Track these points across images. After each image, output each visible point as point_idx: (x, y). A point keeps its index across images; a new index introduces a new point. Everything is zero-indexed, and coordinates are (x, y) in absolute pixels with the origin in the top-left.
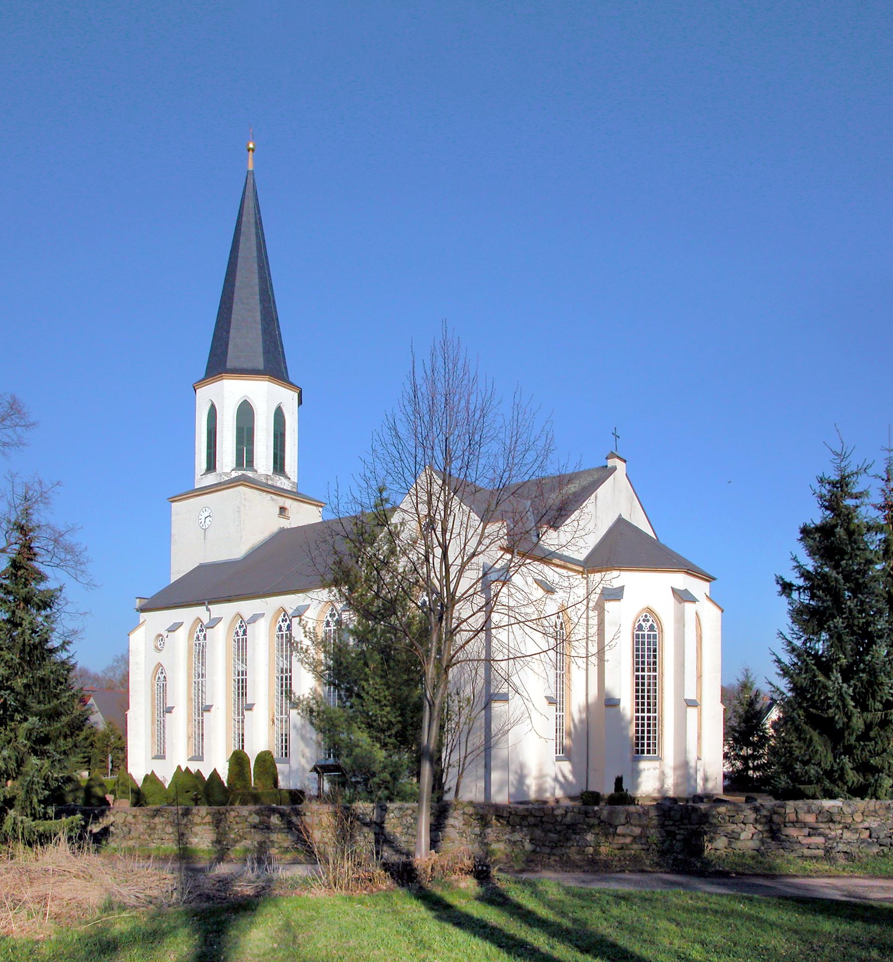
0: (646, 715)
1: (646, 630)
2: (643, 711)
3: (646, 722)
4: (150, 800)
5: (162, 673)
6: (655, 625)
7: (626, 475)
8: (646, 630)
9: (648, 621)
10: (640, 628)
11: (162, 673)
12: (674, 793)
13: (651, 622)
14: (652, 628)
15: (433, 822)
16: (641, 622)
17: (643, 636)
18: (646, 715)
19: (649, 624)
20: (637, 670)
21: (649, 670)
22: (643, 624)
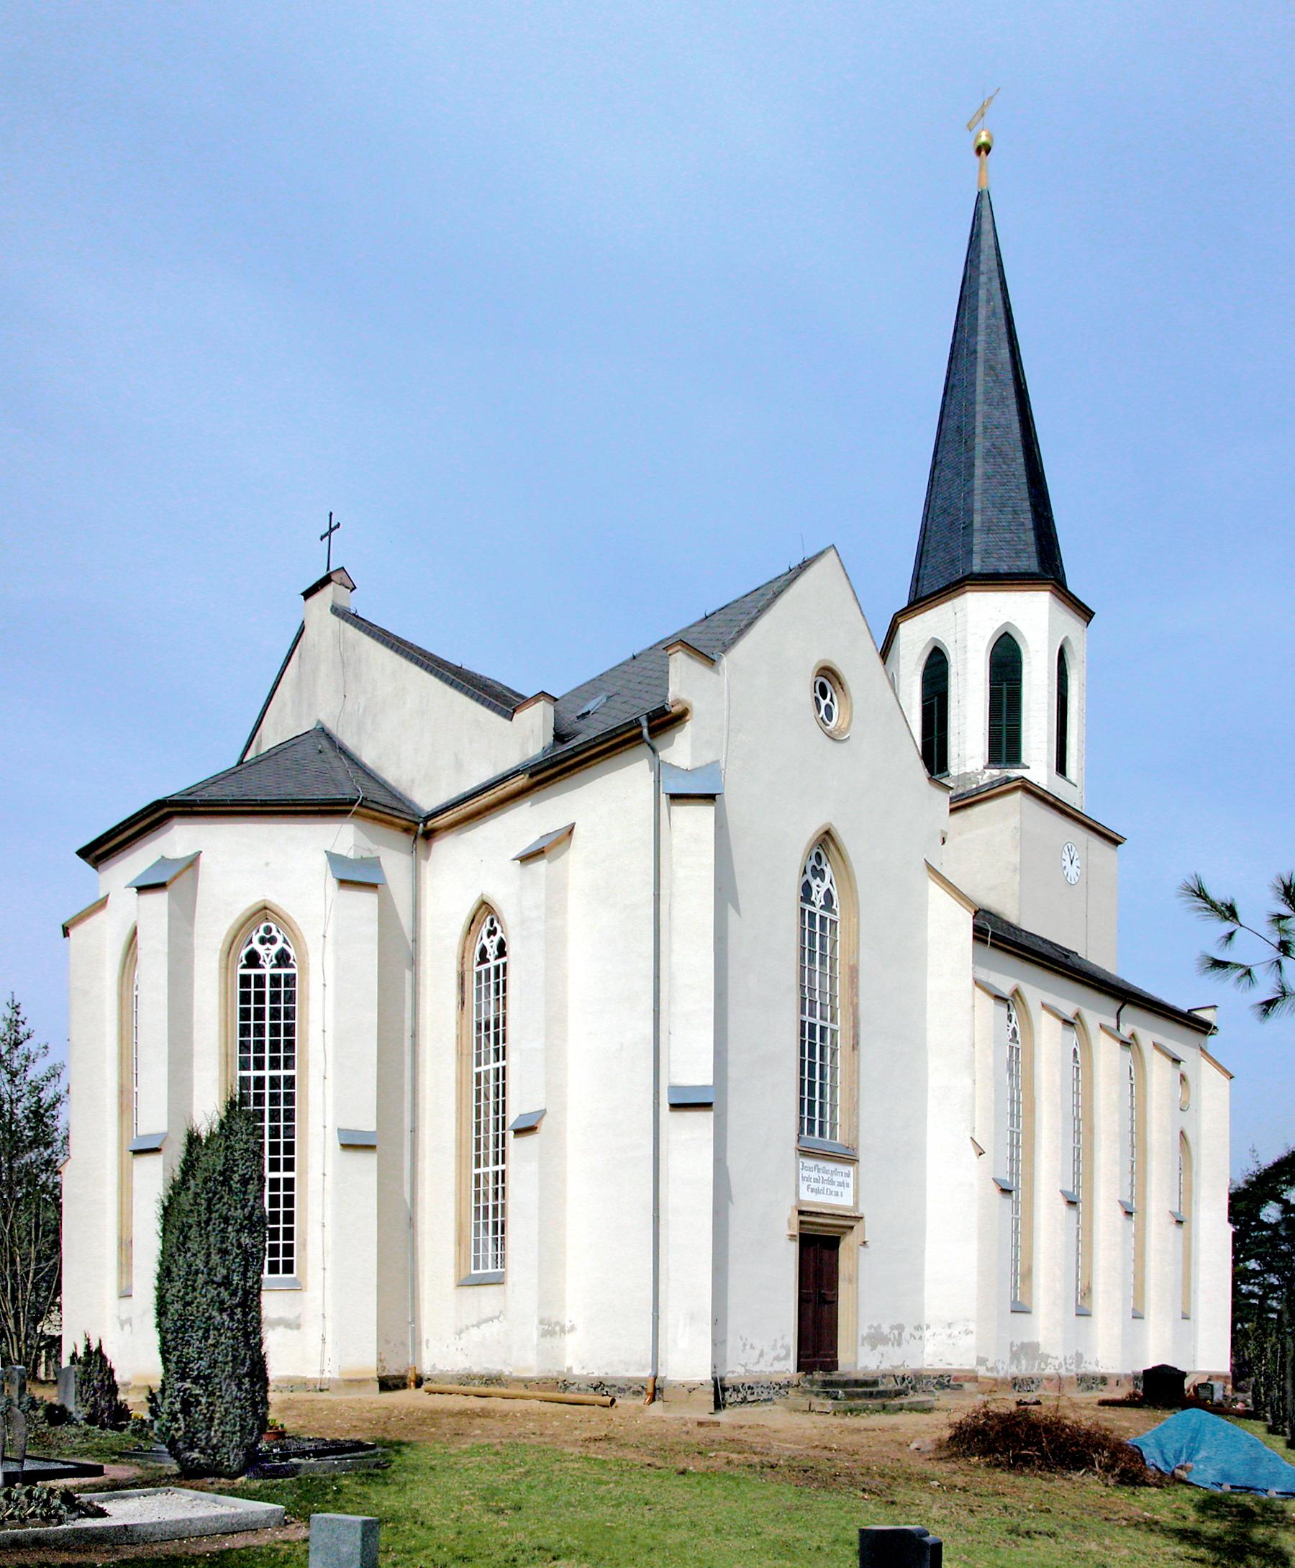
0: (267, 1073)
1: (268, 966)
2: (259, 1064)
3: (267, 1055)
4: (854, 1535)
5: (492, 933)
6: (291, 952)
7: (1077, 954)
8: (268, 966)
9: (273, 941)
10: (253, 960)
11: (492, 933)
12: (340, 1374)
13: (280, 945)
14: (283, 959)
15: (1233, 1362)
16: (256, 945)
17: (260, 980)
18: (267, 1073)
19: (274, 949)
20: (244, 1065)
21: (275, 1064)
22: (261, 949)
